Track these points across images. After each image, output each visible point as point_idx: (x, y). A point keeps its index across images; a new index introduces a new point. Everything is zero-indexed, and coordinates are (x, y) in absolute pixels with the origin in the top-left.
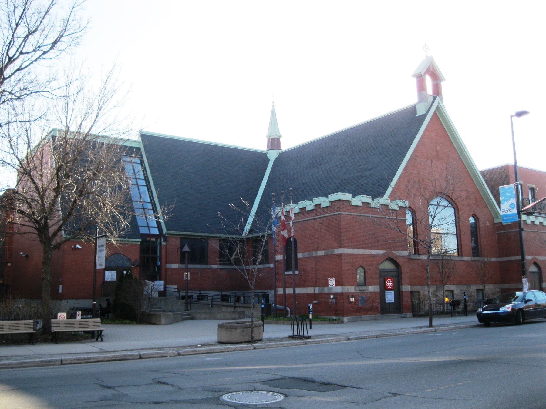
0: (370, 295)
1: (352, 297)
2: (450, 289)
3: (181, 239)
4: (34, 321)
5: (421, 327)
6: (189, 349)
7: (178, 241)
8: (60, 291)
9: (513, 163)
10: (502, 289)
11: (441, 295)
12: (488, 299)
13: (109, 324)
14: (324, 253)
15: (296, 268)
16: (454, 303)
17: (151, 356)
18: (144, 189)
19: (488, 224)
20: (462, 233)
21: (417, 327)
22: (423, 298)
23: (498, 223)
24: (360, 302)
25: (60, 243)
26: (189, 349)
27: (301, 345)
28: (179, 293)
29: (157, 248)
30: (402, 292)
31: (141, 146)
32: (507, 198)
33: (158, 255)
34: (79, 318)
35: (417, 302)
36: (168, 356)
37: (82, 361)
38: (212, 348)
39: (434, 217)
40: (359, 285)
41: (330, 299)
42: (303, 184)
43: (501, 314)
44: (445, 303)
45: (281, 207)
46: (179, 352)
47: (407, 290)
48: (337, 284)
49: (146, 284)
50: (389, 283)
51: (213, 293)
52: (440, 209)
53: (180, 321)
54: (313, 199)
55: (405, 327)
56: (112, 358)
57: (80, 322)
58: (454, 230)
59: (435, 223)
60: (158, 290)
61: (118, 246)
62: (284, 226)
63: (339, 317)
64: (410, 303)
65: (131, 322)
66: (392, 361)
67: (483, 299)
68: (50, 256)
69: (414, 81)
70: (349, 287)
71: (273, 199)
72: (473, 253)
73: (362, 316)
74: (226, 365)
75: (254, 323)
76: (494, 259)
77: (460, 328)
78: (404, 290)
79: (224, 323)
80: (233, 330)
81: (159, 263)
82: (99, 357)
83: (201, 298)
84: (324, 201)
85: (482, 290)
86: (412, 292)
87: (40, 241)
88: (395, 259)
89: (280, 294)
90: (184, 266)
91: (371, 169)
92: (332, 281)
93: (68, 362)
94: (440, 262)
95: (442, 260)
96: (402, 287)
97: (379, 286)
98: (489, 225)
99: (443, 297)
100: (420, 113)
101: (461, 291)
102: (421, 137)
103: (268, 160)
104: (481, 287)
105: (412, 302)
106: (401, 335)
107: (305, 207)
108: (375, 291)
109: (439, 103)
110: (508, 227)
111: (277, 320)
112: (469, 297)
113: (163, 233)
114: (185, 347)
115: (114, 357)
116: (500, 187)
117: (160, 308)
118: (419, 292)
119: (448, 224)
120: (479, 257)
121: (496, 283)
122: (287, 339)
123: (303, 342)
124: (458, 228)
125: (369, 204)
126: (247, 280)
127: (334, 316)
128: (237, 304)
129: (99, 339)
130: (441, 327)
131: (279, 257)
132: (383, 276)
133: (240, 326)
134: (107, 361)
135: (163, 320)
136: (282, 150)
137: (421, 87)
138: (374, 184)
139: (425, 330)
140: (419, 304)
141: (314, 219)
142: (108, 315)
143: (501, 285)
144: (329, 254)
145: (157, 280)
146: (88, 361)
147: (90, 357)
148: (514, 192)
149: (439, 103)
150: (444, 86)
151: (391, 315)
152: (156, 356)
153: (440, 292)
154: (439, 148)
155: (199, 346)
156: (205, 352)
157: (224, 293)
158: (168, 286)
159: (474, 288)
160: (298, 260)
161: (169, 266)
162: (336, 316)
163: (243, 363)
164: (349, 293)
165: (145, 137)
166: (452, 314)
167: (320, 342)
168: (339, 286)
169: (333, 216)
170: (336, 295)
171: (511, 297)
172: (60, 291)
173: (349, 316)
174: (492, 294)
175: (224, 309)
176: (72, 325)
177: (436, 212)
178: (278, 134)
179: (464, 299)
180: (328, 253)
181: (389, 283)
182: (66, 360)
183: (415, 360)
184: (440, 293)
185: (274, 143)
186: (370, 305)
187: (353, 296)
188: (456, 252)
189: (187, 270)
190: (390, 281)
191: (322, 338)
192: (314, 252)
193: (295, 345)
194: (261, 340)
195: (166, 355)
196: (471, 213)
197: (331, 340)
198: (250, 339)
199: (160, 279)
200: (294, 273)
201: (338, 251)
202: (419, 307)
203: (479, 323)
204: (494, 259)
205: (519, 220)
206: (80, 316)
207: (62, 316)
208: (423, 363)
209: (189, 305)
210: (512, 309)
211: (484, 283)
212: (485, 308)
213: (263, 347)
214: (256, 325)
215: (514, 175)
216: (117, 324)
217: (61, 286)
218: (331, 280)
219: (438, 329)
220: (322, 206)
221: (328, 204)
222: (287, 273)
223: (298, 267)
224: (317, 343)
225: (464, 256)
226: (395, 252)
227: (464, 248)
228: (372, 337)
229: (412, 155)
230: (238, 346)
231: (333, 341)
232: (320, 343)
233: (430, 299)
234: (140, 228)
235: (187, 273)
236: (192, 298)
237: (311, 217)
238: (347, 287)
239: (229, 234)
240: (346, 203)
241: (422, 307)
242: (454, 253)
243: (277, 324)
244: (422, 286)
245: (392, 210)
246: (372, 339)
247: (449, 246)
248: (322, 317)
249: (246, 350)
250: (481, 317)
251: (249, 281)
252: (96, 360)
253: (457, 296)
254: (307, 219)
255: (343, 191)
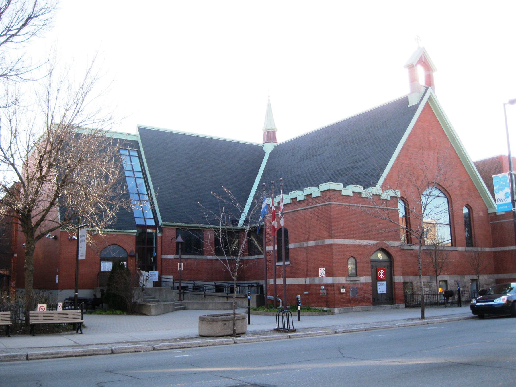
0: (362, 285)
1: (343, 287)
2: (444, 280)
3: (176, 231)
4: (11, 313)
5: (412, 319)
6: (167, 343)
7: (174, 232)
8: (57, 281)
9: (506, 154)
10: (496, 279)
11: (435, 285)
12: (482, 290)
13: (100, 314)
14: (315, 244)
15: (287, 258)
16: (448, 294)
17: (123, 351)
18: (141, 182)
19: (481, 214)
20: (455, 222)
21: (409, 319)
22: (416, 289)
23: (492, 213)
24: (351, 293)
25: (44, 233)
26: (167, 343)
27: (285, 338)
28: (173, 283)
29: (153, 239)
30: (394, 282)
31: (139, 140)
32: (502, 187)
33: (154, 246)
34: (60, 310)
35: (409, 292)
36: (142, 351)
37: (49, 356)
38: (190, 342)
39: (426, 206)
40: (350, 276)
41: (321, 289)
42: (297, 175)
43: (496, 306)
44: (438, 293)
45: (272, 197)
46: (155, 346)
47: (400, 281)
48: (328, 274)
49: (141, 274)
50: (381, 274)
51: (208, 284)
52: (431, 198)
53: (171, 312)
54: (304, 189)
55: (397, 319)
56: (82, 352)
57: (59, 314)
58: (447, 220)
59: (426, 212)
60: (154, 280)
61: (104, 236)
62: (274, 217)
63: (329, 308)
64: (403, 294)
65: (122, 313)
66: (373, 363)
67: (477, 290)
68: (32, 246)
69: (407, 71)
70: (340, 278)
71: (263, 189)
72: (466, 243)
73: (354, 307)
74: (191, 365)
75: (236, 316)
76: (488, 249)
77: (453, 320)
78: (396, 281)
79: (205, 316)
80: (215, 323)
81: (154, 254)
82: (68, 352)
83: (196, 288)
84: (315, 191)
85: (476, 280)
86: (405, 283)
87: (23, 231)
88: (387, 250)
89: (271, 285)
90: (177, 257)
91: (363, 160)
92: (322, 272)
93: (34, 357)
94: (433, 253)
95: (436, 250)
96: (394, 278)
97: (371, 277)
98: (483, 215)
99: (436, 288)
100: (412, 103)
101: (455, 281)
102: (414, 127)
103: (264, 153)
104: (475, 277)
105: (404, 293)
106: (392, 328)
107: (296, 198)
108: (367, 282)
109: (431, 93)
110: (502, 217)
111: (267, 311)
112: (463, 287)
113: (159, 224)
114: (163, 341)
115: (84, 351)
116: (493, 176)
117: (154, 298)
118: (412, 282)
119: (440, 213)
120: (473, 247)
121: (490, 274)
122: (271, 332)
123: (287, 336)
124: (451, 217)
125: (360, 193)
126: (229, 272)
127: (325, 307)
128: (230, 295)
129: (79, 331)
130: (433, 319)
131: (270, 248)
132: (375, 267)
133: (221, 319)
134: (76, 356)
135: (153, 311)
136: (277, 143)
137: (413, 79)
138: (366, 174)
139: (416, 323)
140: (412, 294)
141: (305, 209)
142: (102, 305)
143: (496, 275)
144: (320, 244)
145: (152, 270)
146: (55, 356)
147: (58, 352)
148: (508, 181)
149: (431, 93)
150: (436, 77)
151: (383, 306)
152: (129, 350)
153: (433, 282)
154: (431, 138)
155: (178, 339)
156: (182, 346)
157: (218, 283)
158: (163, 276)
159: (468, 278)
160: (290, 251)
161: (164, 256)
162: (327, 307)
163: (211, 362)
164: (339, 284)
165: (143, 131)
166: (445, 305)
167: (306, 336)
168: (330, 276)
169: (324, 206)
170: (326, 285)
171: (505, 288)
172: (57, 281)
173: (340, 307)
174: (487, 284)
175: (217, 300)
176: (51, 316)
177: (427, 200)
178: (273, 127)
179: (458, 289)
180: (319, 243)
181: (381, 274)
182: (32, 355)
183: (399, 362)
184: (434, 284)
185: (270, 136)
186: (361, 296)
187: (344, 286)
188: (450, 243)
189: (180, 260)
190: (382, 271)
191: (308, 331)
192: (305, 243)
193: (279, 339)
194: (244, 333)
195: (140, 350)
196: (465, 204)
197: (318, 333)
198: (232, 332)
199: (156, 270)
200: (284, 263)
201: (328, 241)
202: (413, 298)
203: (472, 315)
204: (488, 249)
205: (510, 172)
206: (61, 307)
207: (42, 307)
208: (407, 367)
209: (182, 294)
210: (508, 301)
211: (478, 273)
212: (479, 299)
213: (245, 341)
214: (238, 318)
215: (508, 165)
216: (108, 314)
217: (57, 276)
218: (322, 270)
219: (429, 321)
220: (313, 196)
221: (318, 194)
222: (277, 264)
223: (289, 258)
224: (302, 337)
225: (458, 246)
226: (387, 242)
227: (458, 239)
228: (361, 330)
229: (404, 145)
230: (218, 340)
231: (320, 334)
232: (305, 337)
233: (421, 290)
234: (136, 219)
235: (181, 263)
236: (187, 288)
237: (302, 207)
238: (338, 278)
239: (212, 224)
240: (337, 193)
241: (416, 297)
242: (448, 244)
243: (267, 315)
244: (415, 277)
245: (383, 200)
246: (361, 332)
247: (442, 236)
248: (314, 308)
249: (226, 344)
250: (474, 309)
251: (231, 273)
252: (64, 355)
253: (451, 286)
254: (297, 209)
255: (335, 181)
